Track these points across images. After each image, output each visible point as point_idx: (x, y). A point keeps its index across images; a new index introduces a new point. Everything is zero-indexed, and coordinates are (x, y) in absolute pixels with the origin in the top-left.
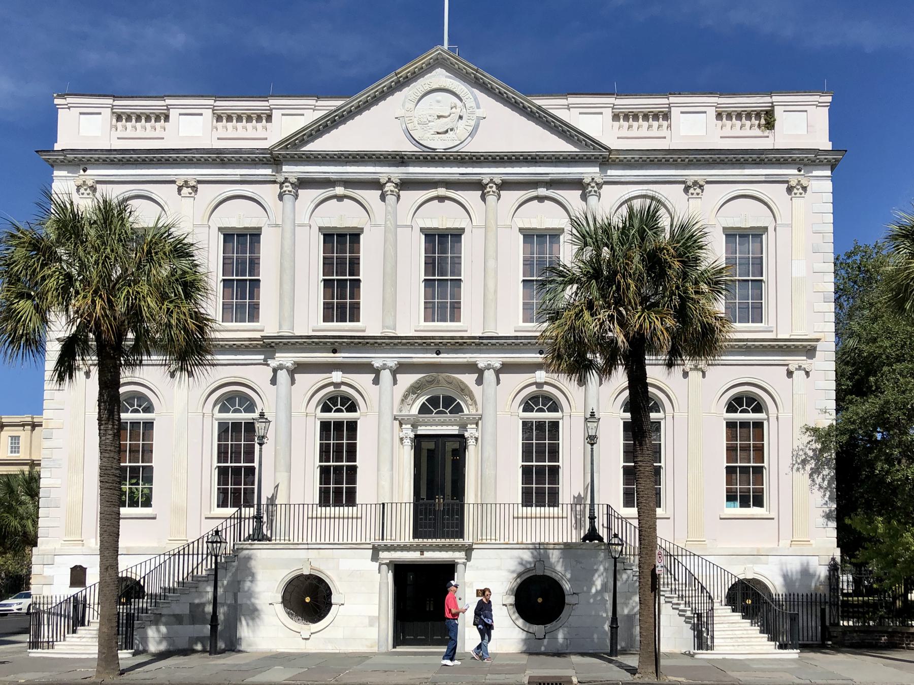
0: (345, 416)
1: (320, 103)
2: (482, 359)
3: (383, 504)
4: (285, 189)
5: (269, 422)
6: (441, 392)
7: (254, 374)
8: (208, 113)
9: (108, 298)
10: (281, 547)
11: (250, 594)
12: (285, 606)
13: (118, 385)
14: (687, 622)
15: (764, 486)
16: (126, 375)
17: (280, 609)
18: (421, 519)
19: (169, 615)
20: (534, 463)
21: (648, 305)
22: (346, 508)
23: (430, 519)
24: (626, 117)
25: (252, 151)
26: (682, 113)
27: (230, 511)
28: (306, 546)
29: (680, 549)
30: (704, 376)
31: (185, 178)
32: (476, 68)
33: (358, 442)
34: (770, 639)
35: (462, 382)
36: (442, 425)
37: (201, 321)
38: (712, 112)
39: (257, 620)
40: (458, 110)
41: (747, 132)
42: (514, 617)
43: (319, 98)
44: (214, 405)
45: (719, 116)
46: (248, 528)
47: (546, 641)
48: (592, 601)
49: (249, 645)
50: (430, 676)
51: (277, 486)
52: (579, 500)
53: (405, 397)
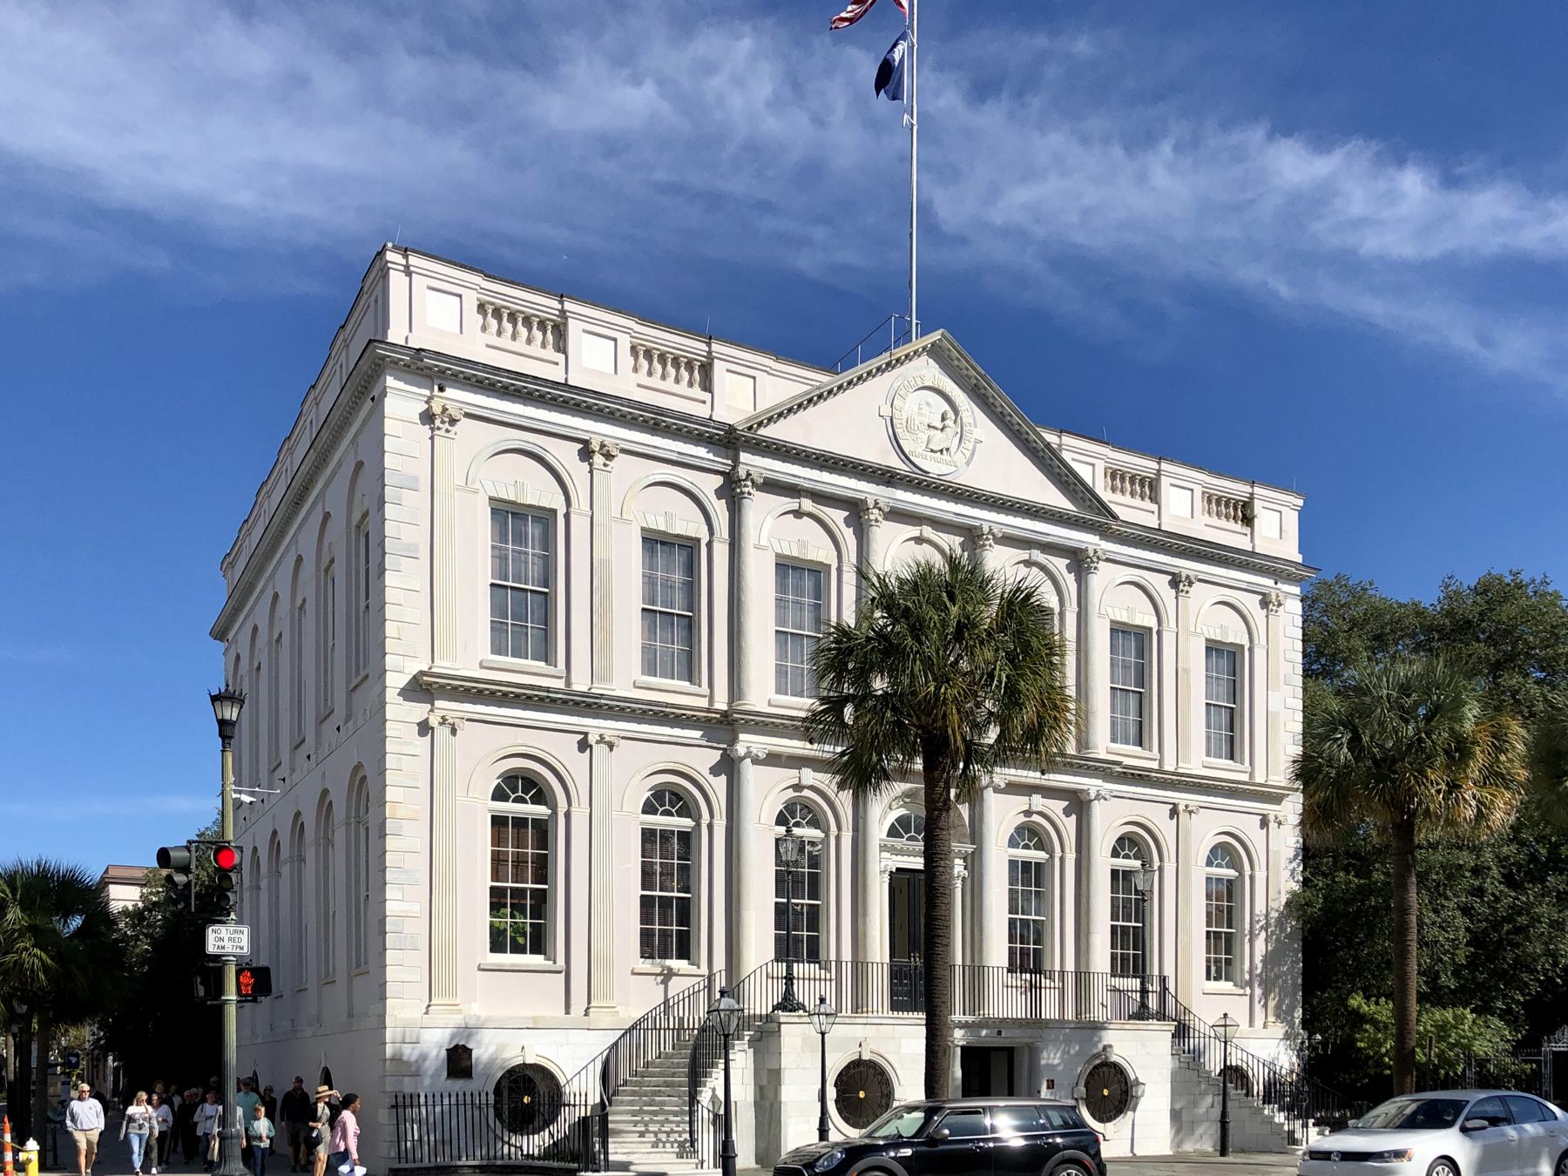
41: (1223, 523)
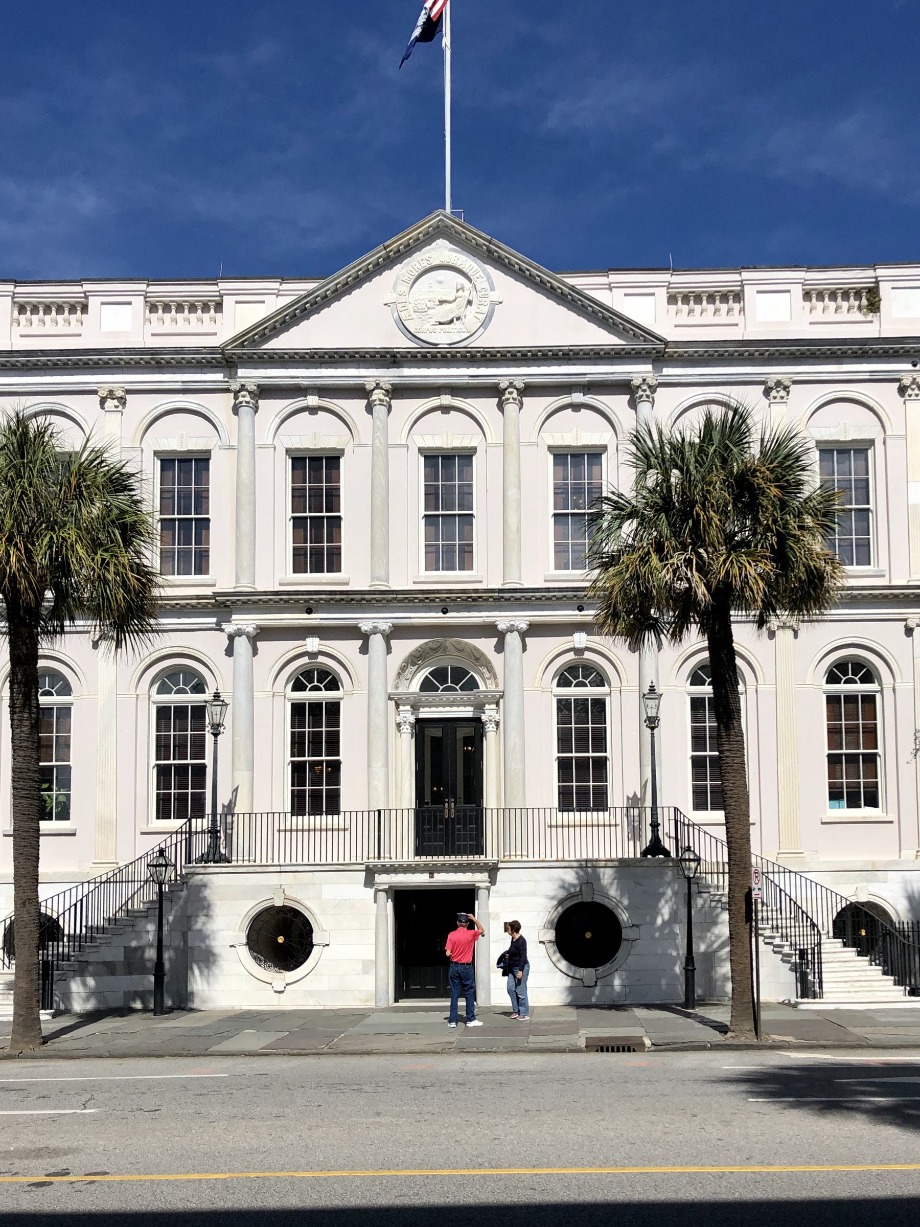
0: (324, 695)
1: (285, 286)
2: (502, 619)
3: (379, 811)
4: (241, 399)
5: (227, 705)
6: (448, 662)
7: (203, 642)
8: (139, 302)
9: (26, 547)
10: (245, 870)
11: (203, 936)
12: (250, 949)
13: (36, 657)
14: (784, 962)
15: (879, 780)
16: (45, 646)
17: (244, 952)
18: (459, 830)
19: (98, 963)
20: (574, 754)
21: (733, 545)
22: (577, 814)
23: (471, 829)
24: (686, 299)
25: (197, 351)
26: (758, 292)
27: (175, 824)
28: (278, 869)
29: (770, 865)
30: (796, 636)
31: (110, 387)
32: (489, 238)
33: (342, 729)
34: (896, 983)
35: (477, 649)
36: (451, 706)
37: (145, 576)
38: (798, 291)
39: (214, 968)
40: (467, 293)
41: (844, 316)
42: (554, 958)
43: (283, 279)
44: (152, 684)
45: (807, 296)
46: (201, 845)
47: (597, 991)
48: (657, 935)
49: (204, 1002)
50: (453, 1039)
51: (236, 790)
52: (634, 802)
53: (403, 669)
